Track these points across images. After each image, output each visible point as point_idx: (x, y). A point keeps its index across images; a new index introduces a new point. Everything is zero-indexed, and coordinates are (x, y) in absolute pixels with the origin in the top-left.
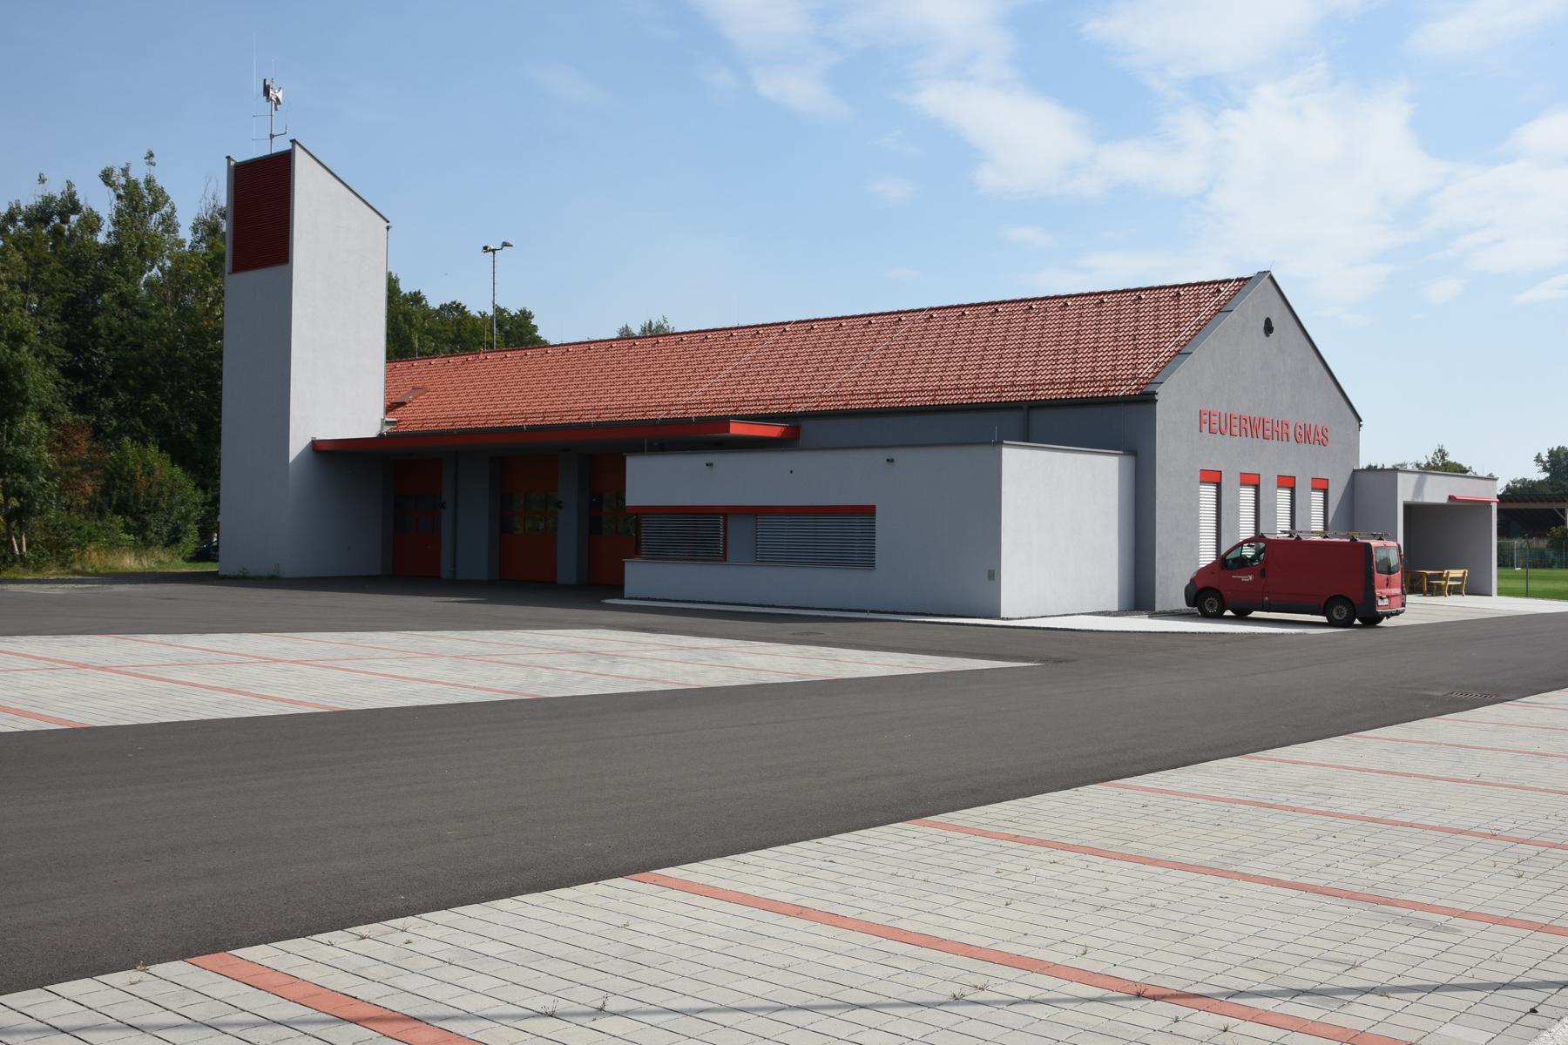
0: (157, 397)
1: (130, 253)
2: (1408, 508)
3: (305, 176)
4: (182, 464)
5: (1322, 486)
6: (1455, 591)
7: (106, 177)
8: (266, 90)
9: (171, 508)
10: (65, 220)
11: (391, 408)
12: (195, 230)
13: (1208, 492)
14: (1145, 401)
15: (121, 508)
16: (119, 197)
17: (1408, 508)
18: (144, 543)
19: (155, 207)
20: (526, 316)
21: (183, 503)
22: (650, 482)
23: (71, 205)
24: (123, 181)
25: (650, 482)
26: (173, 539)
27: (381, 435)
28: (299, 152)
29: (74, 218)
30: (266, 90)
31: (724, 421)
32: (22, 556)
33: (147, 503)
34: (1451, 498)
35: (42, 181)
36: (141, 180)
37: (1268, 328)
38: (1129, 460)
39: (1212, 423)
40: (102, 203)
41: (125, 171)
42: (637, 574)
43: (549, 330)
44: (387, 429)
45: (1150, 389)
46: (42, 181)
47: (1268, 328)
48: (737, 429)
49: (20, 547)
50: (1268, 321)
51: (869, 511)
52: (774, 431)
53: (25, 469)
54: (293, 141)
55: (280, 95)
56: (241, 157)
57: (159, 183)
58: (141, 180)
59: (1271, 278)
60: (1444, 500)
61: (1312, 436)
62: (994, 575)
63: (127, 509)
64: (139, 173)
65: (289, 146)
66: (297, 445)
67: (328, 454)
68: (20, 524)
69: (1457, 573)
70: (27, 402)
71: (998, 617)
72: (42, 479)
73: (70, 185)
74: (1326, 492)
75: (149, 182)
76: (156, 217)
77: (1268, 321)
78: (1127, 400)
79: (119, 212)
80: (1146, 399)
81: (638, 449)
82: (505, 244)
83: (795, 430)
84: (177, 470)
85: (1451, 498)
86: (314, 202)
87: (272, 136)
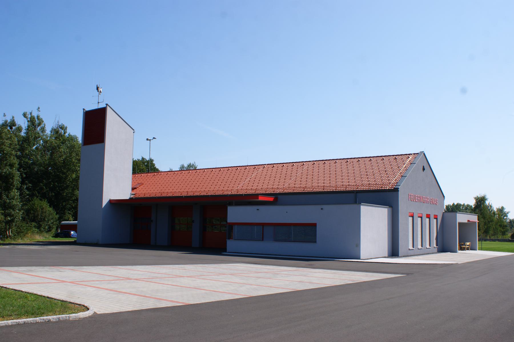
0: (41, 184)
1: (31, 139)
2: (459, 223)
3: (110, 116)
4: (54, 208)
5: (436, 217)
6: (468, 249)
7: (25, 115)
8: (97, 88)
9: (48, 220)
10: (11, 128)
11: (133, 189)
12: (51, 132)
13: (411, 218)
14: (395, 191)
15: (33, 221)
16: (28, 121)
17: (459, 223)
18: (40, 232)
19: (39, 124)
20: (151, 161)
21: (52, 219)
22: (235, 214)
23: (13, 124)
24: (29, 116)
25: (235, 214)
26: (49, 230)
27: (131, 199)
28: (108, 108)
29: (14, 128)
30: (97, 88)
31: (256, 196)
32: (10, 236)
33: (41, 219)
34: (468, 221)
35: (5, 115)
36: (36, 116)
37: (424, 169)
38: (390, 209)
39: (412, 199)
40: (23, 123)
41: (31, 113)
42: (231, 244)
43: (161, 165)
44: (132, 196)
45: (397, 187)
46: (5, 115)
47: (424, 169)
48: (261, 199)
49: (9, 233)
50: (423, 167)
51: (315, 225)
52: (271, 199)
53: (13, 208)
54: (107, 104)
55: (101, 90)
56: (88, 109)
57: (41, 117)
58: (36, 116)
59: (424, 154)
60: (466, 221)
61: (433, 203)
62: (358, 245)
63: (33, 219)
64: (35, 114)
65: (105, 106)
66: (105, 202)
67: (114, 204)
68: (9, 225)
69: (468, 244)
70: (14, 186)
71: (360, 259)
72: (18, 211)
73: (13, 117)
74: (437, 219)
75: (38, 117)
76: (39, 128)
77: (423, 167)
78: (389, 191)
79: (28, 126)
80: (396, 190)
81: (231, 204)
82: (154, 138)
83: (277, 199)
84: (51, 209)
85: (468, 221)
86: (112, 125)
87: (98, 103)
